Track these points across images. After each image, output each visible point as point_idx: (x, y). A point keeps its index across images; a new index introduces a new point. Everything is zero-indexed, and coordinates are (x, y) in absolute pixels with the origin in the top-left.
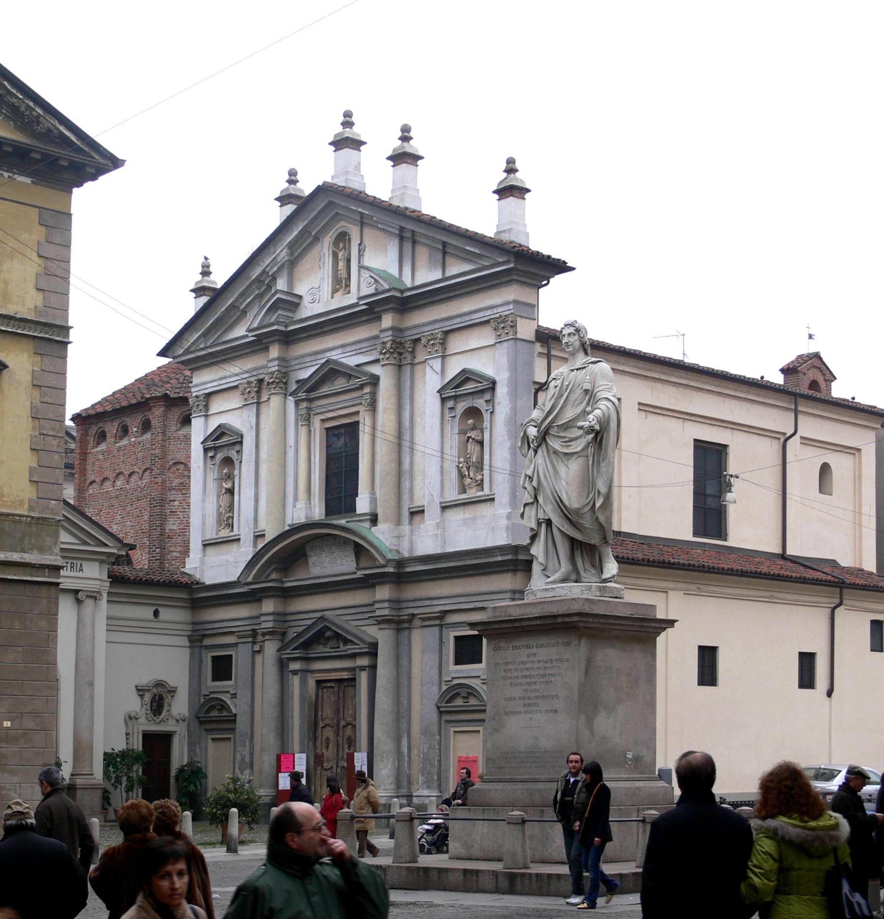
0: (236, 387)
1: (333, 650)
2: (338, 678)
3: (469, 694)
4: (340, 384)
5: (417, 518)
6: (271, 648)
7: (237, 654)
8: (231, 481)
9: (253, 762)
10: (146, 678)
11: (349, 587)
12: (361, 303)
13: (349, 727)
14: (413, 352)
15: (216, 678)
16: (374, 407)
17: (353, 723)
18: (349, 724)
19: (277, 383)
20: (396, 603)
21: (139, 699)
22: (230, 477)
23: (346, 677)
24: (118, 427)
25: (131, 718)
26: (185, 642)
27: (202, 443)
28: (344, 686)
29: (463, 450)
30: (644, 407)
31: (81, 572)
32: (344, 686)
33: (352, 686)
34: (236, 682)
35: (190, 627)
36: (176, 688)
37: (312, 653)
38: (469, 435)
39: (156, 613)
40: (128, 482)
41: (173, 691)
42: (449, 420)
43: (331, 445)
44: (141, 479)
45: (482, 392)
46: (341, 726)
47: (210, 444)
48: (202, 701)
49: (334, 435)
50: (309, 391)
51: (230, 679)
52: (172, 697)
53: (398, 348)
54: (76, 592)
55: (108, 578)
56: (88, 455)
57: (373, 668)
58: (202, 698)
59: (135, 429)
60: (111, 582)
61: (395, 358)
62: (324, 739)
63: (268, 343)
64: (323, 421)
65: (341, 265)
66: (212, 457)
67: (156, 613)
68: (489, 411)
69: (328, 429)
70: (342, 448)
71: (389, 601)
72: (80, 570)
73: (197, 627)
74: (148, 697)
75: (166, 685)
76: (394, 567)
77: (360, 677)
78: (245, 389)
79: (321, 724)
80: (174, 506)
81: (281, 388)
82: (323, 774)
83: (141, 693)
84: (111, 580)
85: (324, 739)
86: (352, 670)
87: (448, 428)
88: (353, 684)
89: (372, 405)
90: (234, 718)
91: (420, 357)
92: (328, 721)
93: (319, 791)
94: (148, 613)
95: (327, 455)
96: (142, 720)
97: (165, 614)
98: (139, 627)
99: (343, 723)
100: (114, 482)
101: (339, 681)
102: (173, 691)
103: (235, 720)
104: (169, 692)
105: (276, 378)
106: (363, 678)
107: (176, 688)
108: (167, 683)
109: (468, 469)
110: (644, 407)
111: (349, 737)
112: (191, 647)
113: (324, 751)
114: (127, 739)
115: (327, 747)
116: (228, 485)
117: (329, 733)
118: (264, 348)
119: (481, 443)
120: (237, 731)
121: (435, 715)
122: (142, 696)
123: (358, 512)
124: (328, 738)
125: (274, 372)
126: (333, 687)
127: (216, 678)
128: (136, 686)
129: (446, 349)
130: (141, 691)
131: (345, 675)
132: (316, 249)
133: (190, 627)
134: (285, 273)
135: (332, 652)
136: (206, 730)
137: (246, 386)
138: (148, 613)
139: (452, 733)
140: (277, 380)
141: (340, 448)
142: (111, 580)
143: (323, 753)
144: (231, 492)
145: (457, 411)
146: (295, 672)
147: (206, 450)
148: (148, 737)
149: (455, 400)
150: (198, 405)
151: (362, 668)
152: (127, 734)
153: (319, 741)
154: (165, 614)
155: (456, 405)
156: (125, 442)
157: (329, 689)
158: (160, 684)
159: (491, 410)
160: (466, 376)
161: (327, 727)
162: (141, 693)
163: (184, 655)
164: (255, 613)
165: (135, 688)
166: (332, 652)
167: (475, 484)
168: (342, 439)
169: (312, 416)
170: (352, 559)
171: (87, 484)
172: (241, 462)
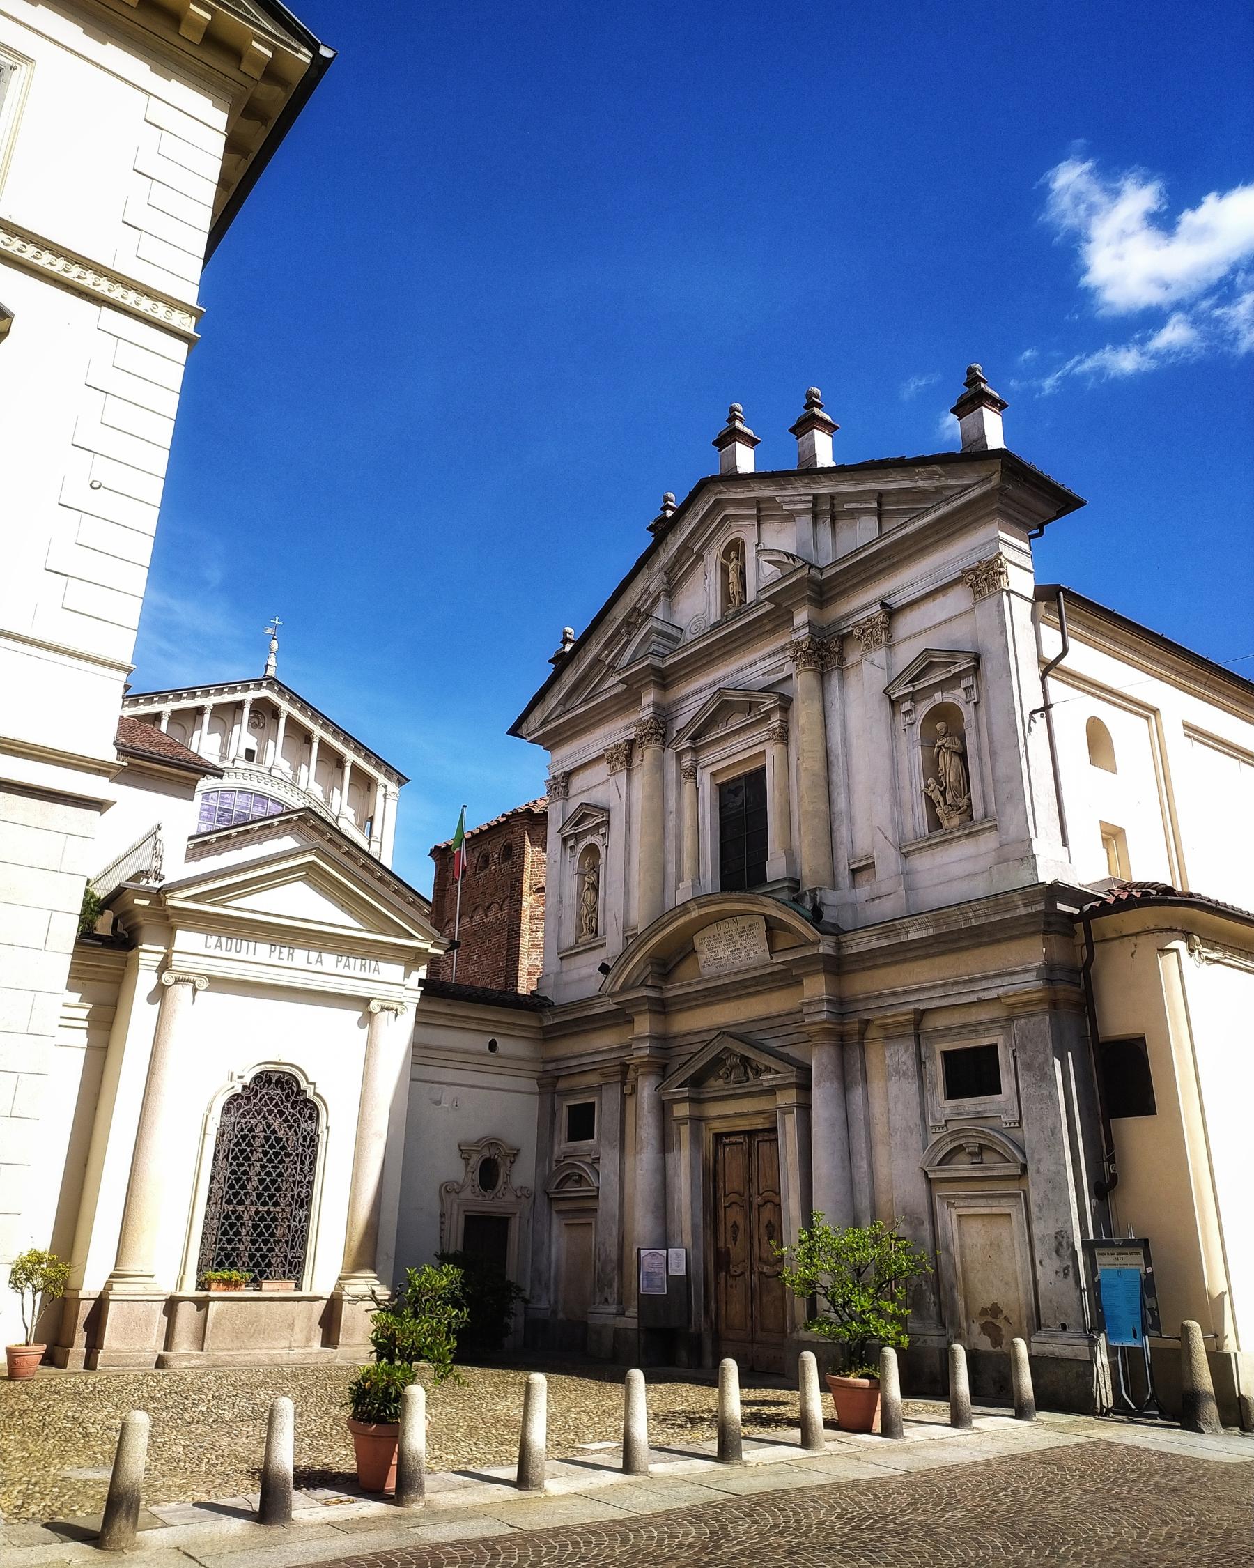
0: (603, 756)
1: (739, 1085)
2: (747, 1128)
3: (981, 1147)
4: (737, 721)
5: (864, 876)
6: (646, 1090)
7: (600, 1099)
8: (595, 875)
9: (622, 1260)
10: (476, 1130)
11: (760, 988)
12: (763, 597)
13: (769, 1206)
14: (841, 653)
15: (572, 1137)
16: (787, 740)
17: (776, 1201)
18: (769, 1201)
19: (652, 734)
20: (841, 1005)
21: (463, 1163)
22: (594, 868)
23: (760, 1127)
24: (479, 857)
25: (447, 1189)
26: (533, 1086)
27: (559, 832)
28: (758, 1142)
29: (932, 768)
30: (1192, 731)
31: (376, 973)
32: (758, 1142)
33: (770, 1141)
34: (599, 1140)
35: (539, 1067)
36: (518, 1150)
37: (708, 1092)
38: (939, 743)
39: (493, 1046)
40: (486, 916)
41: (515, 1154)
42: (905, 730)
43: (726, 805)
44: (500, 909)
45: (958, 677)
46: (755, 1206)
47: (569, 831)
48: (554, 1168)
49: (730, 791)
50: (694, 738)
51: (592, 1138)
52: (512, 1163)
53: (819, 649)
54: (367, 1001)
55: (419, 985)
56: (446, 892)
57: (805, 1109)
58: (554, 1164)
59: (496, 856)
60: (422, 991)
61: (815, 662)
62: (729, 1225)
63: (639, 687)
64: (713, 774)
65: (733, 577)
66: (572, 848)
67: (493, 1046)
68: (972, 703)
69: (721, 786)
70: (742, 805)
71: (828, 1001)
72: (374, 970)
73: (550, 1067)
74: (476, 1160)
75: (498, 1142)
76: (833, 947)
77: (784, 1124)
78: (612, 756)
79: (724, 1202)
80: (537, 938)
81: (656, 740)
82: (729, 1284)
83: (465, 1156)
84: (422, 989)
85: (729, 1225)
86: (773, 1113)
87: (904, 742)
88: (772, 1137)
89: (783, 736)
90: (594, 1194)
91: (853, 657)
92: (734, 1197)
93: (724, 1312)
94: (482, 1043)
95: (721, 819)
96: (467, 1194)
97: (504, 1045)
98: (465, 1060)
99: (757, 1200)
100: (472, 917)
101: (750, 1134)
102: (515, 1154)
103: (597, 1197)
104: (507, 1155)
105: (651, 728)
106: (789, 1128)
107: (518, 1150)
108: (499, 1140)
109: (943, 793)
110: (1192, 731)
111: (770, 1222)
112: (540, 1094)
113: (730, 1246)
114: (442, 1223)
115: (735, 1239)
116: (593, 879)
117: (736, 1215)
118: (634, 702)
119: (963, 756)
120: (599, 1212)
121: (922, 1185)
122: (467, 1160)
123: (768, 881)
124: (735, 1225)
125: (648, 721)
126: (741, 1143)
127: (572, 1137)
128: (459, 1146)
129: (891, 636)
130: (465, 1152)
131: (759, 1123)
132: (700, 568)
133: (539, 1067)
134: (663, 600)
135: (736, 1088)
136: (559, 1212)
137: (614, 752)
138: (482, 1043)
139: (954, 1217)
140: (652, 731)
141: (740, 806)
142: (422, 989)
143: (728, 1250)
144: (594, 887)
145: (918, 715)
146: (681, 1121)
147: (565, 840)
148: (473, 1222)
149: (912, 700)
150: (555, 788)
151: (787, 1110)
152: (442, 1215)
153: (721, 1229)
154: (504, 1045)
155: (914, 706)
156: (486, 871)
157: (735, 1147)
158: (493, 1143)
159: (976, 700)
160: (929, 662)
161: (734, 1206)
162: (465, 1156)
163: (532, 1105)
164: (626, 1039)
165: (457, 1148)
166: (736, 1088)
167: (959, 812)
168: (742, 794)
169: (699, 769)
170: (763, 948)
171: (444, 923)
172: (607, 847)
